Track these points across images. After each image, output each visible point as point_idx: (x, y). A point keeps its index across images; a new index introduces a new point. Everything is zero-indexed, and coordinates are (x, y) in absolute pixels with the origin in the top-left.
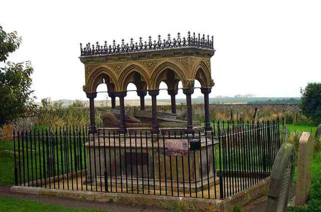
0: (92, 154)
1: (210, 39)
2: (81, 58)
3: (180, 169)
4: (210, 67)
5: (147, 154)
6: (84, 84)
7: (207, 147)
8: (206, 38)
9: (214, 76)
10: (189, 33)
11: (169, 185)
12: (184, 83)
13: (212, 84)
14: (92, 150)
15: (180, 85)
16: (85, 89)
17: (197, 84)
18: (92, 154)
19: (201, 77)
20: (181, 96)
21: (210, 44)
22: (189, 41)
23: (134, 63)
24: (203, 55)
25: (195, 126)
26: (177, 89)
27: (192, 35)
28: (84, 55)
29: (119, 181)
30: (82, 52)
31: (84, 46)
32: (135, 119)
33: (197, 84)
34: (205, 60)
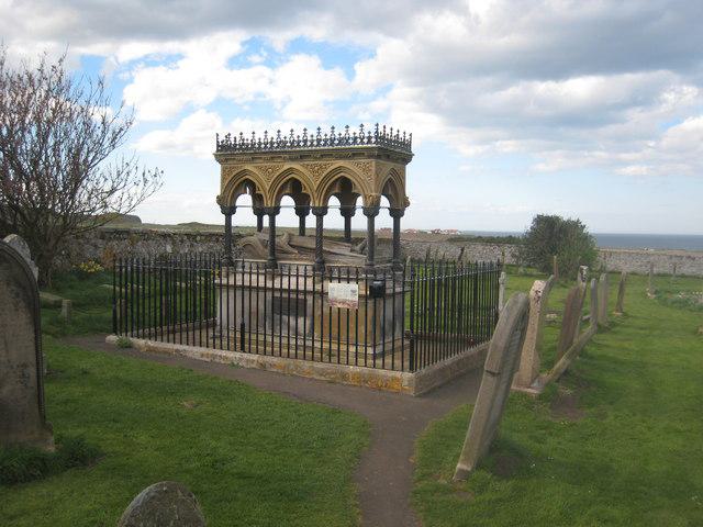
0: (224, 294)
1: (408, 137)
2: (216, 155)
3: (352, 325)
4: (404, 178)
5: (305, 300)
6: (218, 192)
7: (394, 294)
8: (401, 135)
9: (410, 190)
10: (377, 125)
11: (334, 347)
12: (365, 198)
13: (407, 204)
14: (224, 290)
15: (360, 201)
16: (220, 200)
17: (384, 202)
18: (224, 294)
19: (390, 193)
20: (311, 221)
21: (407, 145)
22: (376, 137)
23: (293, 166)
24: (396, 161)
25: (378, 263)
26: (354, 209)
27: (381, 130)
28: (221, 151)
29: (261, 338)
30: (218, 146)
31: (222, 138)
32: (291, 249)
33: (384, 202)
34: (397, 166)
